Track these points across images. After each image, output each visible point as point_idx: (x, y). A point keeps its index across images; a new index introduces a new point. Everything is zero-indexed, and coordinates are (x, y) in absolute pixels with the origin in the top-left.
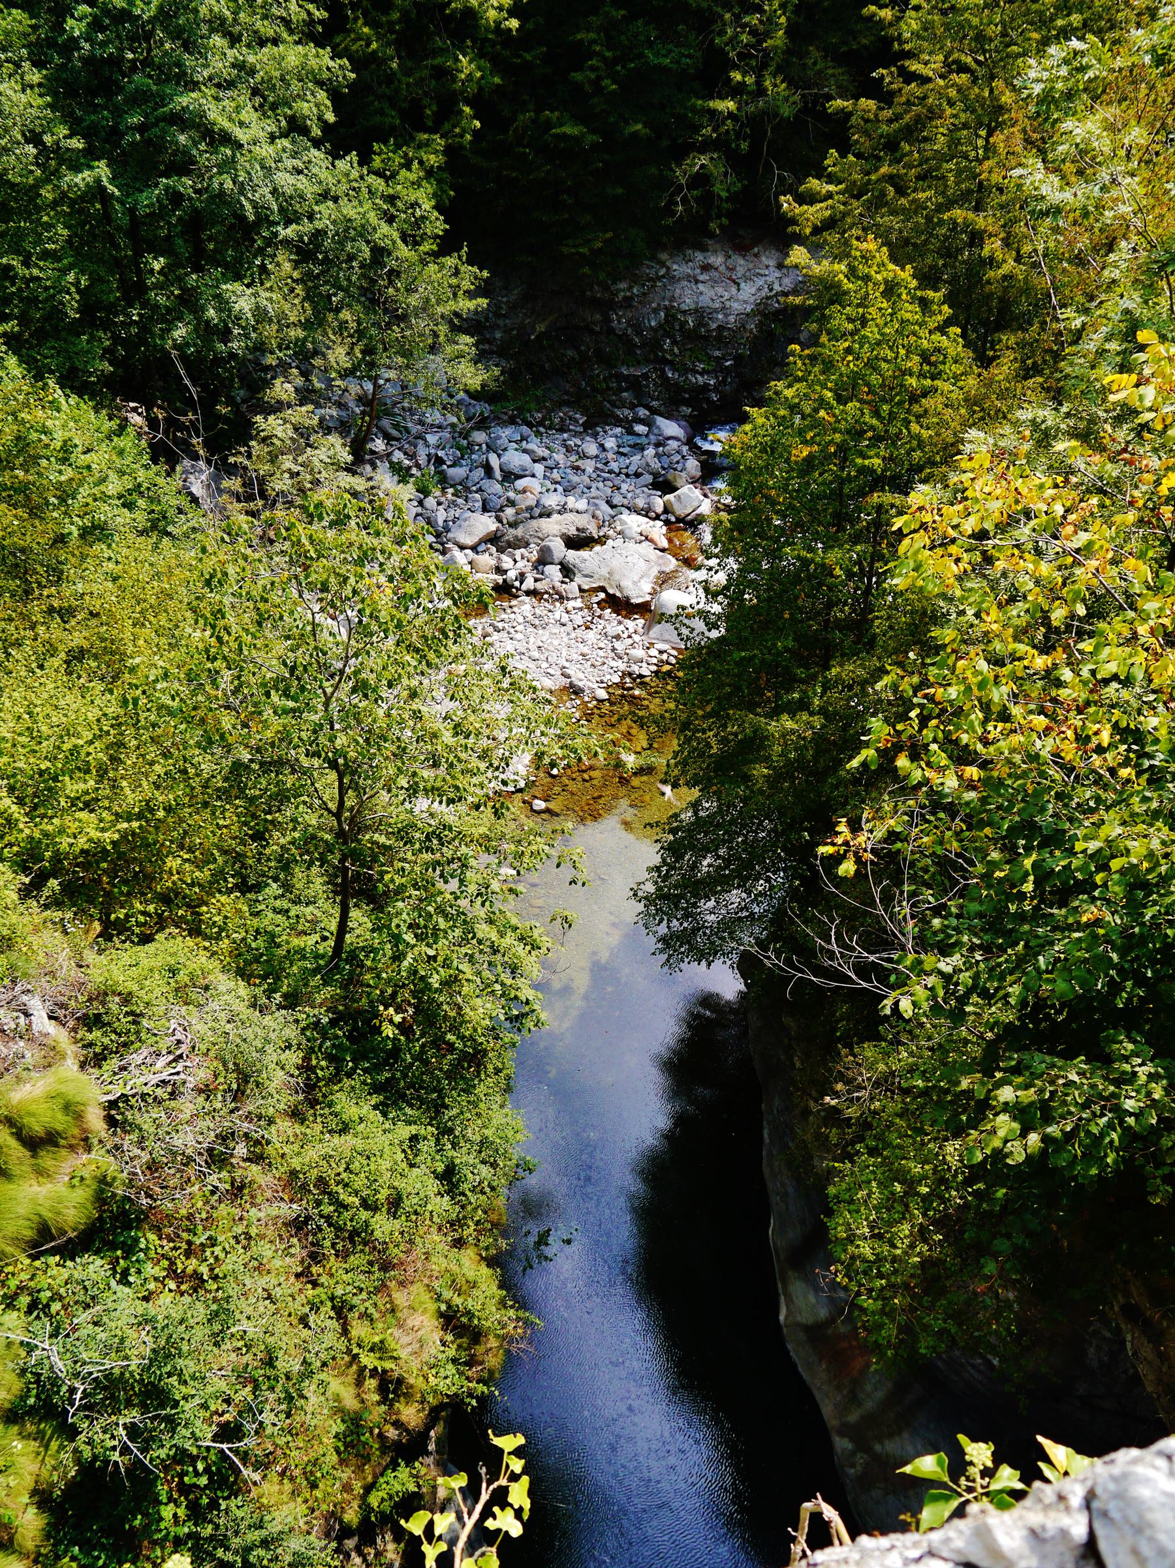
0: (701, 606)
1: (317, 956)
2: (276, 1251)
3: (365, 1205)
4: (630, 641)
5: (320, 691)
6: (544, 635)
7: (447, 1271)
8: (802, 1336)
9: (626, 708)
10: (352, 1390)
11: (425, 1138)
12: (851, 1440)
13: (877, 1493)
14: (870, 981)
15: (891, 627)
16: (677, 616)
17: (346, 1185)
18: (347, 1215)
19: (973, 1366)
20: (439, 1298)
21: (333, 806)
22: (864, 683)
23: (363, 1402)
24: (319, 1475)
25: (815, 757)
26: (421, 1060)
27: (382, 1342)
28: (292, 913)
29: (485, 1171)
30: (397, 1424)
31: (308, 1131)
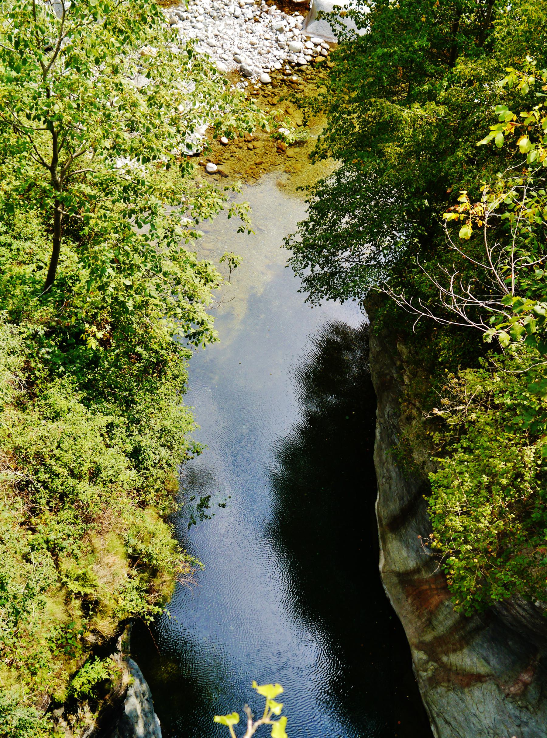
0: (353, 7)
1: (34, 282)
2: (5, 505)
3: (72, 474)
4: (291, 34)
5: (38, 64)
6: (220, 25)
7: (133, 524)
8: (395, 580)
9: (285, 90)
10: (62, 608)
11: (118, 426)
12: (426, 653)
13: (441, 690)
14: (478, 322)
15: (509, 33)
16: (333, 14)
17: (58, 459)
18: (58, 481)
19: (520, 606)
20: (127, 544)
21: (48, 161)
22: (481, 80)
23: (70, 616)
24: (37, 666)
25: (439, 139)
26: (116, 366)
27: (84, 574)
28: (14, 247)
29: (164, 452)
30: (94, 632)
31: (29, 417)
